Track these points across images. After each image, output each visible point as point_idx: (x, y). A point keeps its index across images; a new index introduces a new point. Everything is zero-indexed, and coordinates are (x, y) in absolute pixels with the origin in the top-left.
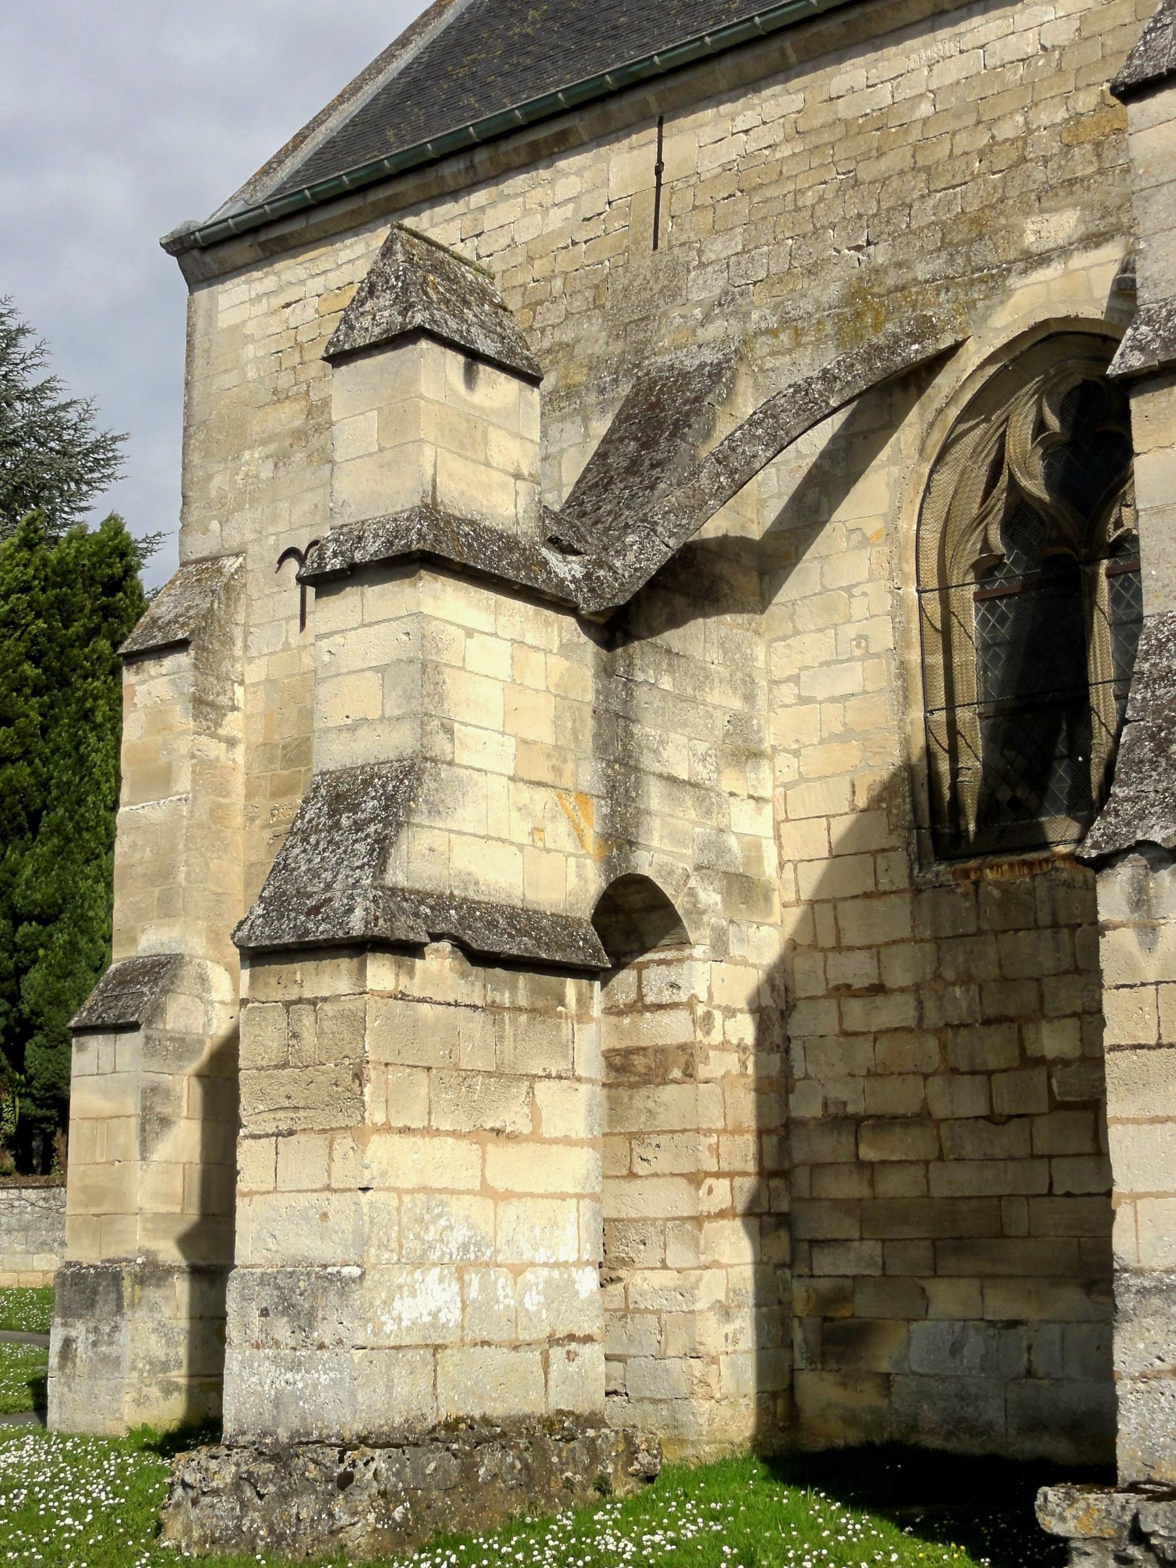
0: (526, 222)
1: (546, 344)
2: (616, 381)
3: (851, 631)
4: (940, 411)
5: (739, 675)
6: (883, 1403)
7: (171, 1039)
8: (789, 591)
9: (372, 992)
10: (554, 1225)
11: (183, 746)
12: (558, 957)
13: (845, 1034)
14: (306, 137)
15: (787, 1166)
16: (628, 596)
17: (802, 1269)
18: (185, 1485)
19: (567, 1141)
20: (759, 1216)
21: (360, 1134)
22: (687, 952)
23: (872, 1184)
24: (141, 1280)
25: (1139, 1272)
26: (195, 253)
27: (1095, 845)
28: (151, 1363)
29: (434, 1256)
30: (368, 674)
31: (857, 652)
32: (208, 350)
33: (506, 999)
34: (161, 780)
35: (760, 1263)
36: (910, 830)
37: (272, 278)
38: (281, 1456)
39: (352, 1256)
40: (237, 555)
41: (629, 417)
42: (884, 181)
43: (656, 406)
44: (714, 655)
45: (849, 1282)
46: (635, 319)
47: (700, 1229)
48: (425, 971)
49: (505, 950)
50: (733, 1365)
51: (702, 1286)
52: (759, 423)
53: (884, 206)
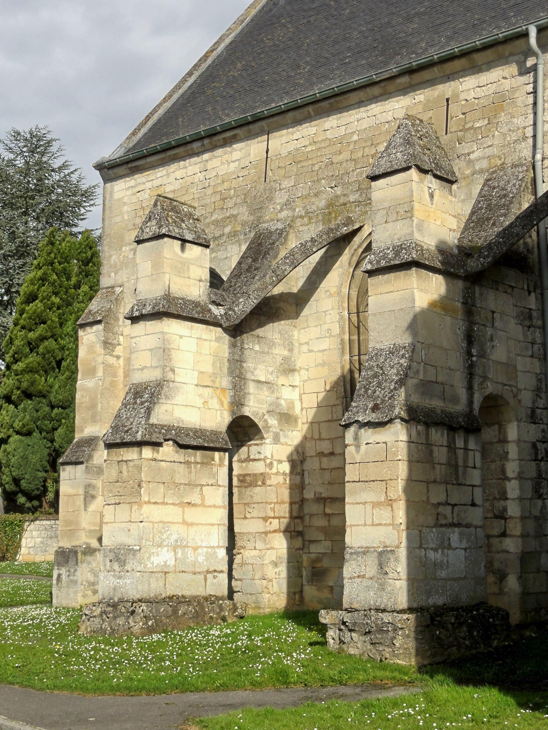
0: (222, 167)
1: (228, 215)
2: (250, 231)
3: (326, 327)
4: (356, 250)
5: (287, 342)
6: (330, 596)
7: (95, 467)
8: (306, 311)
9: (144, 459)
10: (209, 534)
11: (100, 359)
12: (211, 445)
13: (322, 469)
14: (150, 118)
15: (302, 515)
16: (239, 321)
17: (306, 550)
18: (86, 615)
19: (214, 506)
20: (290, 532)
21: (140, 504)
22: (264, 441)
23: (329, 521)
24: (84, 553)
25: (351, 548)
26: (105, 170)
27: (345, 421)
28: (88, 583)
29: (165, 544)
30: (147, 351)
31: (328, 335)
32: (111, 207)
33: (193, 460)
34: (92, 372)
35: (289, 548)
36: (343, 398)
37: (133, 181)
38: (115, 606)
39: (137, 543)
40: (121, 286)
41: (251, 248)
42: (341, 163)
43: (260, 244)
44: (277, 336)
45: (321, 555)
46: (257, 209)
47: (267, 536)
48: (163, 451)
49: (194, 443)
50: (278, 583)
51: (267, 555)
52: (288, 258)
53: (341, 172)
